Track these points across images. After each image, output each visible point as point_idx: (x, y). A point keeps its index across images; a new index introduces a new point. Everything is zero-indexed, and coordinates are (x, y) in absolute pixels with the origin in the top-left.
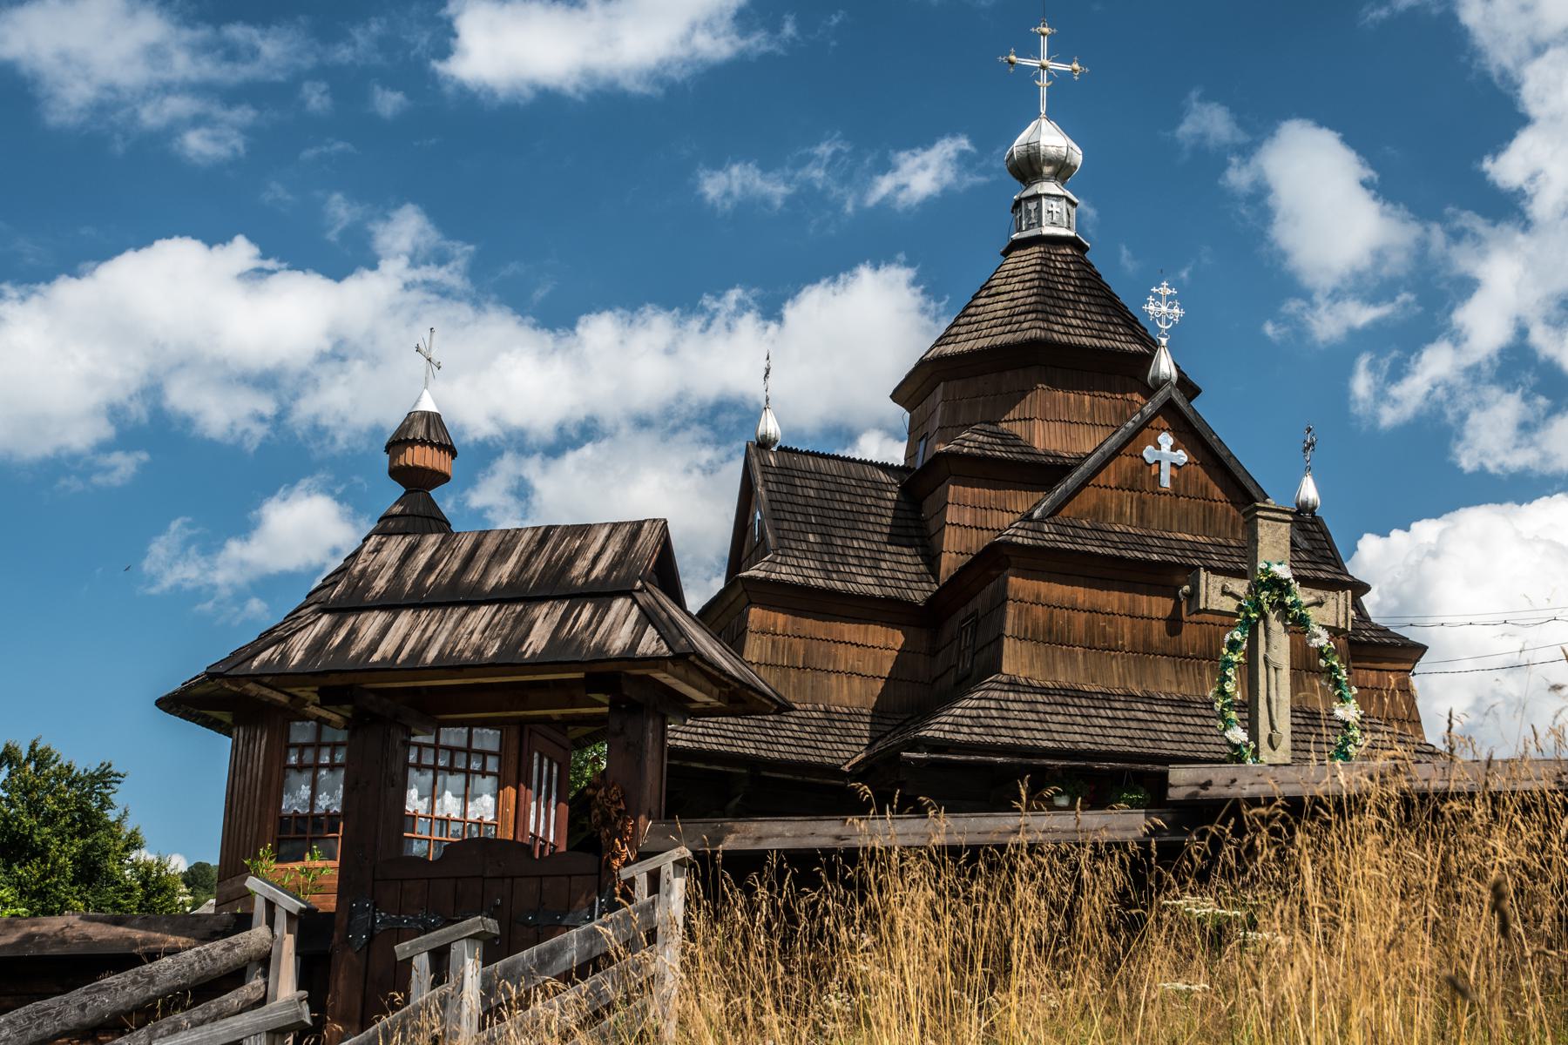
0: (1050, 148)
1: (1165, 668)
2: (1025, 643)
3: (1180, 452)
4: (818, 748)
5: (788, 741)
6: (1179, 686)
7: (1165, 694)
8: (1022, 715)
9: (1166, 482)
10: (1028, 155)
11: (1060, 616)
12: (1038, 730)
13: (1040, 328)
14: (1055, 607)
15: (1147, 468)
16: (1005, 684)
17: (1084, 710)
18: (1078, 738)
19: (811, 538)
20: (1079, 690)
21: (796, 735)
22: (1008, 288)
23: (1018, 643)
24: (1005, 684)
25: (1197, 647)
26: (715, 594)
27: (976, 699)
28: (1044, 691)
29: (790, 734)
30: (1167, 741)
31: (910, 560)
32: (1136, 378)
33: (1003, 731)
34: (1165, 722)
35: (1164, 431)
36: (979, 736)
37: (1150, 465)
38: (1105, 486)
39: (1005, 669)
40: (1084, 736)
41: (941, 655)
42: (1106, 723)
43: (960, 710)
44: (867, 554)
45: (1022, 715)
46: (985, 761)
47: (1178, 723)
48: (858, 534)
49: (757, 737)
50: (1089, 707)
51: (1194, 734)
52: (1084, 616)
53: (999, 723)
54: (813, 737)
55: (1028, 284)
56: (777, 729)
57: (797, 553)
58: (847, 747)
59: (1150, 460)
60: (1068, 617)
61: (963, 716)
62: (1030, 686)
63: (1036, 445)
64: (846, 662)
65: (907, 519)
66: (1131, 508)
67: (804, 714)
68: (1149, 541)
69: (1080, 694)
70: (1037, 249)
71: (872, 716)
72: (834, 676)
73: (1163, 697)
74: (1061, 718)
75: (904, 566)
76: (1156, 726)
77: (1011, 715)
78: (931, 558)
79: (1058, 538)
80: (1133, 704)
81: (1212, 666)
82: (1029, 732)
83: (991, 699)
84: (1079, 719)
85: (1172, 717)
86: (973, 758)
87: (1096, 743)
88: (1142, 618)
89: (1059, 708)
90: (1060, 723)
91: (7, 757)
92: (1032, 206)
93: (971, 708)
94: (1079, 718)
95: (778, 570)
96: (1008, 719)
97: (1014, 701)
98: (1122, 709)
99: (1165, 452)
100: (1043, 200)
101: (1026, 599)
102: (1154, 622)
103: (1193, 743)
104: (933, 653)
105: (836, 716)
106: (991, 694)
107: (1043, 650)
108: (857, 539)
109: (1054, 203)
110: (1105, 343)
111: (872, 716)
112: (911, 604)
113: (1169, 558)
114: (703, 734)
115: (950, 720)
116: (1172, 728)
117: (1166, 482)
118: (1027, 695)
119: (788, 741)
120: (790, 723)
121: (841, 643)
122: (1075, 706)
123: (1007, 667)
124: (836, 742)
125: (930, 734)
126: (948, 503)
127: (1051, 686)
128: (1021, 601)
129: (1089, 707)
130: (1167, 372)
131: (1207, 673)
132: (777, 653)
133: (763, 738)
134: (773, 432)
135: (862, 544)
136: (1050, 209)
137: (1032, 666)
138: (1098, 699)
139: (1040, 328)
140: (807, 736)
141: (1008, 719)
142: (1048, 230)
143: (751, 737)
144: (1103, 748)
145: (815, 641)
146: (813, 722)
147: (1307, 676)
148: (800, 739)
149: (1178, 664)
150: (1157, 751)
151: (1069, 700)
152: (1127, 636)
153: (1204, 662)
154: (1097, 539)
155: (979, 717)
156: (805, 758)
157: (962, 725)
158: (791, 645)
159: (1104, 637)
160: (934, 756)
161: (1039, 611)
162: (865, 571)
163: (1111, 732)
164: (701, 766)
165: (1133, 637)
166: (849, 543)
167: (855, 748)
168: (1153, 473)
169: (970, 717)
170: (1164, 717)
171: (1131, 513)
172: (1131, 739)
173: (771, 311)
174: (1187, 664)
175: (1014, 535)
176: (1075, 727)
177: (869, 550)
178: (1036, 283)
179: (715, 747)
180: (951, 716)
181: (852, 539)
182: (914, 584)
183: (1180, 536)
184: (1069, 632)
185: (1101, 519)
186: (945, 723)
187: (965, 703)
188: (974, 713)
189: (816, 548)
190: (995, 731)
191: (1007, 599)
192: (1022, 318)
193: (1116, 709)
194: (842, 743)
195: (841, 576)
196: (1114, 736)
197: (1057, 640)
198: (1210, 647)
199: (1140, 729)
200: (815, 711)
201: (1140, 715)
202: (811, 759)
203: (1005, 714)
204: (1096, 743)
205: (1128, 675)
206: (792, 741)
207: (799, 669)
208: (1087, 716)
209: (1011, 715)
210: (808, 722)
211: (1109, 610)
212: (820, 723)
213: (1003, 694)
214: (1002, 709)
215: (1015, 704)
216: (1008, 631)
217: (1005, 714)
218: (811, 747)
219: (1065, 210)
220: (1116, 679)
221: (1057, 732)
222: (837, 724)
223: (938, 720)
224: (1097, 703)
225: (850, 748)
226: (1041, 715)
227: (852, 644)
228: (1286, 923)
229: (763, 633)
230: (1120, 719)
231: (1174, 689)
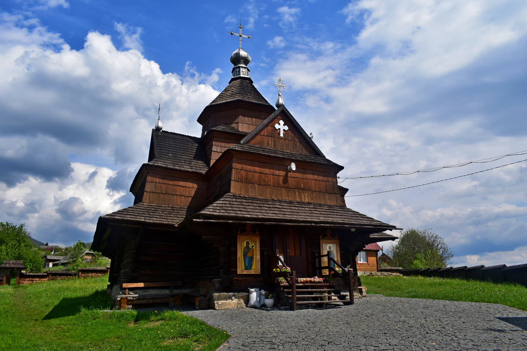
0: (243, 55)
1: (284, 191)
2: (238, 183)
4: (167, 219)
5: (157, 217)
8: (238, 206)
10: (237, 57)
11: (250, 175)
13: (241, 97)
14: (248, 171)
15: (276, 131)
16: (232, 196)
17: (259, 205)
18: (258, 214)
19: (170, 155)
20: (257, 198)
21: (160, 215)
22: (231, 89)
23: (236, 182)
24: (232, 196)
25: (294, 185)
26: (138, 171)
27: (222, 201)
28: (245, 198)
29: (158, 214)
30: (287, 214)
33: (231, 212)
34: (286, 209)
35: (281, 120)
36: (223, 213)
37: (277, 130)
38: (263, 135)
39: (232, 191)
40: (260, 213)
43: (216, 204)
44: (188, 160)
45: (238, 206)
46: (225, 222)
47: (290, 209)
48: (185, 154)
49: (146, 215)
50: (261, 203)
51: (296, 212)
52: (258, 174)
53: (230, 209)
54: (166, 215)
55: (237, 88)
56: (154, 213)
57: (165, 159)
58: (177, 218)
59: (277, 128)
60: (253, 174)
61: (217, 206)
62: (240, 197)
63: (240, 130)
64: (180, 192)
66: (271, 142)
67: (164, 208)
68: (277, 152)
69: (258, 199)
70: (239, 80)
71: (187, 209)
72: (175, 196)
73: (284, 201)
74: (251, 207)
76: (283, 210)
77: (234, 206)
78: (207, 162)
79: (249, 149)
80: (275, 203)
82: (241, 212)
83: (227, 201)
84: (258, 208)
85: (288, 207)
86: (220, 221)
87: (264, 216)
88: (276, 176)
89: (251, 204)
91: (2, 225)
92: (237, 70)
94: (257, 207)
95: (158, 163)
96: (233, 207)
98: (271, 204)
99: (281, 126)
100: (241, 68)
101: (239, 168)
102: (280, 177)
103: (296, 215)
105: (175, 209)
106: (227, 199)
107: (244, 185)
108: (185, 156)
109: (244, 69)
110: (259, 102)
111: (187, 209)
112: (201, 174)
113: (285, 157)
114: (126, 214)
115: (212, 207)
116: (288, 210)
118: (239, 200)
119: (157, 217)
120: (159, 211)
121: (178, 186)
122: (256, 203)
123: (232, 190)
124: (174, 217)
125: (204, 212)
126: (213, 145)
127: (247, 197)
128: (237, 169)
129: (261, 203)
130: (282, 102)
131: (297, 193)
133: (148, 216)
134: (160, 126)
135: (186, 157)
136: (243, 71)
137: (241, 190)
138: (263, 201)
139: (241, 97)
140: (164, 215)
141: (233, 207)
142: (242, 76)
143: (144, 215)
144: (267, 217)
145: (169, 185)
146: (167, 211)
147: (327, 194)
148: (162, 216)
150: (285, 218)
151: (254, 201)
152: (272, 181)
155: (223, 207)
156: (162, 222)
157: (217, 209)
158: (161, 186)
159: (264, 181)
160: (206, 220)
162: (186, 164)
163: (269, 212)
165: (274, 182)
166: (182, 156)
167: (180, 219)
168: (278, 132)
169: (219, 207)
170: (285, 207)
172: (276, 214)
173: (144, 58)
174: (291, 190)
175: (235, 147)
176: (256, 210)
177: (188, 159)
178: (239, 87)
179: (129, 219)
180: (212, 206)
181: (183, 155)
182: (202, 169)
183: (287, 151)
184: (253, 179)
185: (262, 145)
187: (217, 202)
188: (221, 205)
189: (171, 157)
190: (229, 212)
191: (232, 168)
192: (235, 95)
193: (269, 204)
194: (176, 217)
195: (178, 166)
196: (270, 213)
197: (249, 182)
198: (297, 185)
200: (168, 207)
201: (278, 206)
202: (164, 222)
203: (232, 206)
204: (264, 216)
206: (158, 217)
207: (164, 194)
208: (260, 207)
209: (234, 206)
210: (165, 210)
211: (266, 173)
212: (169, 211)
213: (231, 199)
214: (231, 204)
215: (235, 202)
216: (233, 179)
217: (232, 206)
218: (165, 218)
220: (268, 195)
221: (250, 212)
222: (175, 211)
223: (208, 208)
224: (263, 203)
225: (179, 219)
226: (245, 206)
227: (182, 186)
229: (152, 182)
230: (271, 207)
231: (287, 198)
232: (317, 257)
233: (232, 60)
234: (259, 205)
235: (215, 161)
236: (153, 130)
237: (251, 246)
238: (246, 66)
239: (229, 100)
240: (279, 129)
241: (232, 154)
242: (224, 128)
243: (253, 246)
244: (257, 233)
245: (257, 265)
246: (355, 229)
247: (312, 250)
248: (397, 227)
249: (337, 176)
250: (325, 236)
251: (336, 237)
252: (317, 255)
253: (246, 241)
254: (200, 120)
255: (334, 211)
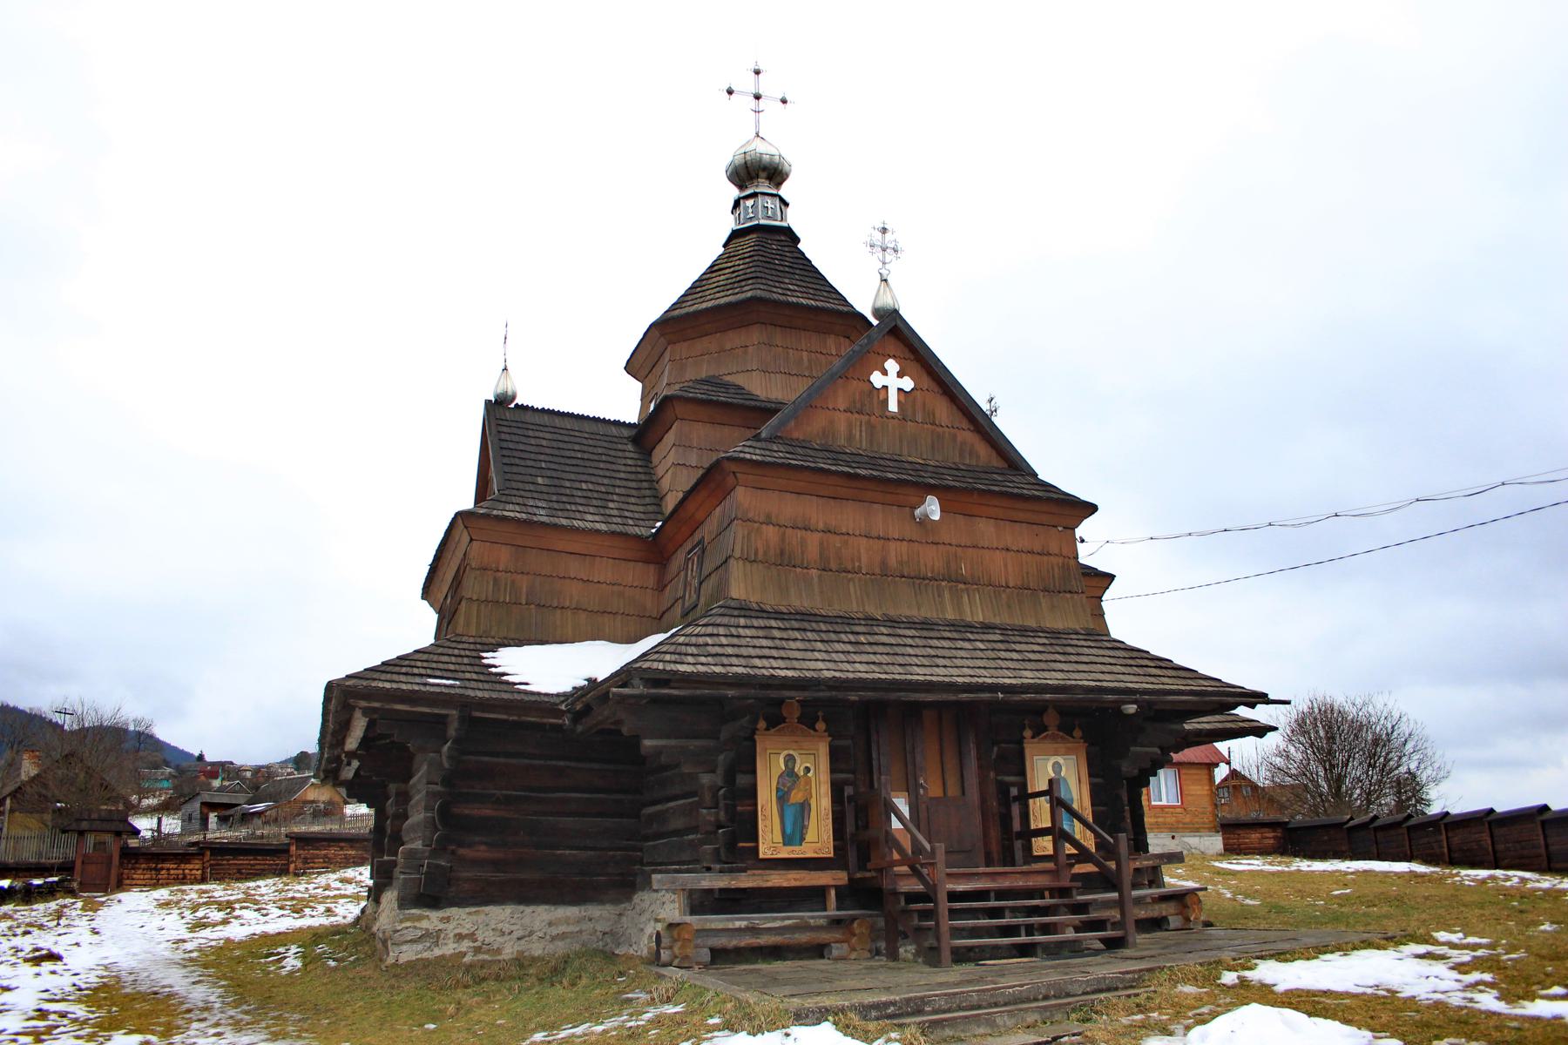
2: (755, 565)
3: (907, 379)
6: (919, 609)
7: (905, 617)
9: (893, 406)
10: (746, 163)
12: (774, 658)
17: (823, 635)
18: (820, 665)
22: (730, 265)
23: (747, 564)
28: (778, 615)
31: (632, 455)
32: (848, 338)
33: (734, 661)
35: (890, 357)
40: (827, 663)
41: (668, 588)
42: (849, 648)
55: (748, 260)
59: (878, 385)
61: (687, 645)
62: (763, 611)
65: (636, 466)
66: (861, 431)
69: (819, 619)
70: (754, 236)
72: (559, 611)
74: (799, 645)
75: (631, 506)
77: (743, 642)
80: (875, 628)
81: (951, 588)
83: (719, 625)
84: (819, 645)
85: (917, 640)
90: (798, 650)
93: (697, 635)
97: (745, 627)
98: (864, 633)
103: (945, 666)
104: (661, 587)
117: (893, 406)
122: (813, 631)
131: (947, 595)
132: (499, 590)
136: (766, 205)
144: (851, 676)
147: (1044, 596)
149: (917, 586)
153: (943, 583)
154: (829, 458)
157: (686, 654)
161: (770, 532)
163: (857, 658)
164: (427, 710)
170: (909, 641)
171: (861, 435)
176: (816, 653)
180: (673, 644)
186: (665, 653)
190: (725, 660)
193: (858, 633)
196: (860, 663)
199: (887, 654)
205: (865, 599)
208: (827, 642)
211: (844, 530)
219: (778, 206)
228: (1382, 1000)
230: (863, 644)
232: (1016, 799)
233: (732, 174)
234: (824, 636)
235: (681, 495)
236: (488, 403)
237: (802, 768)
238: (774, 192)
239: (722, 301)
240: (885, 387)
241: (734, 473)
242: (710, 388)
243: (807, 770)
244: (821, 726)
245: (823, 829)
246: (1135, 706)
247: (999, 778)
248: (1271, 697)
249: (1077, 537)
250: (1039, 730)
251: (1077, 733)
252: (1014, 791)
253: (786, 752)
254: (632, 368)
255: (1070, 650)
